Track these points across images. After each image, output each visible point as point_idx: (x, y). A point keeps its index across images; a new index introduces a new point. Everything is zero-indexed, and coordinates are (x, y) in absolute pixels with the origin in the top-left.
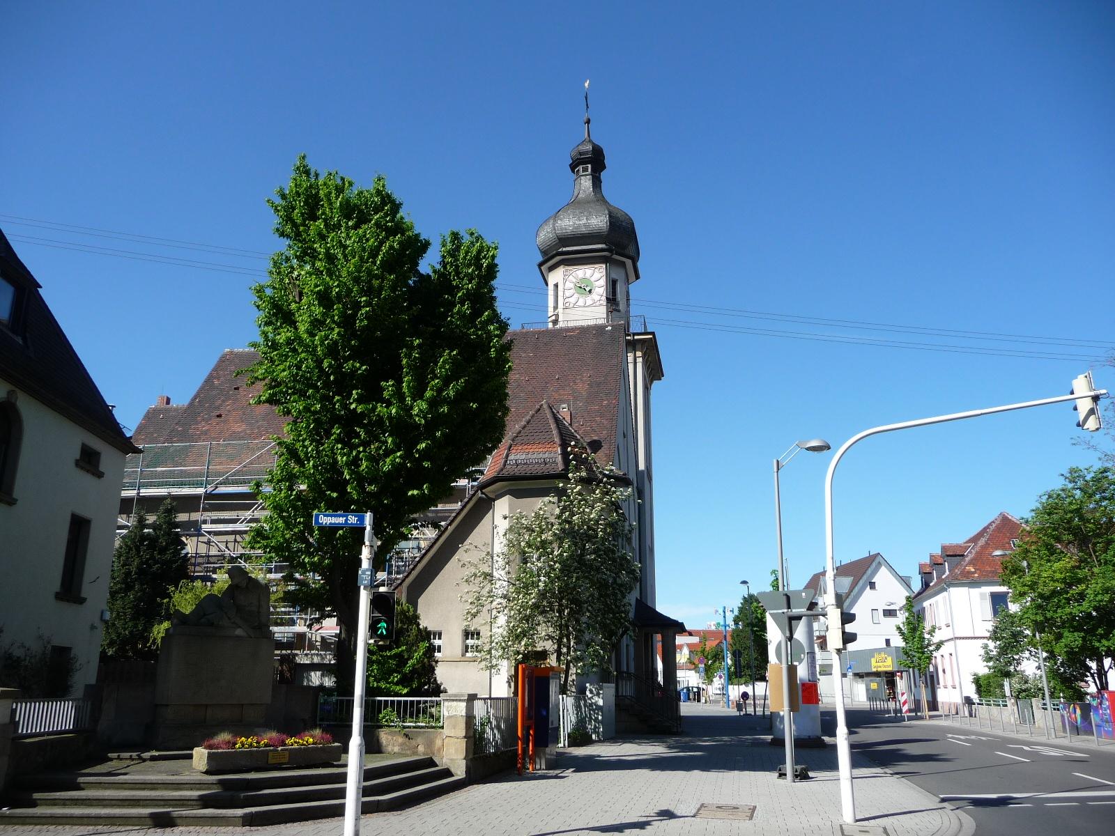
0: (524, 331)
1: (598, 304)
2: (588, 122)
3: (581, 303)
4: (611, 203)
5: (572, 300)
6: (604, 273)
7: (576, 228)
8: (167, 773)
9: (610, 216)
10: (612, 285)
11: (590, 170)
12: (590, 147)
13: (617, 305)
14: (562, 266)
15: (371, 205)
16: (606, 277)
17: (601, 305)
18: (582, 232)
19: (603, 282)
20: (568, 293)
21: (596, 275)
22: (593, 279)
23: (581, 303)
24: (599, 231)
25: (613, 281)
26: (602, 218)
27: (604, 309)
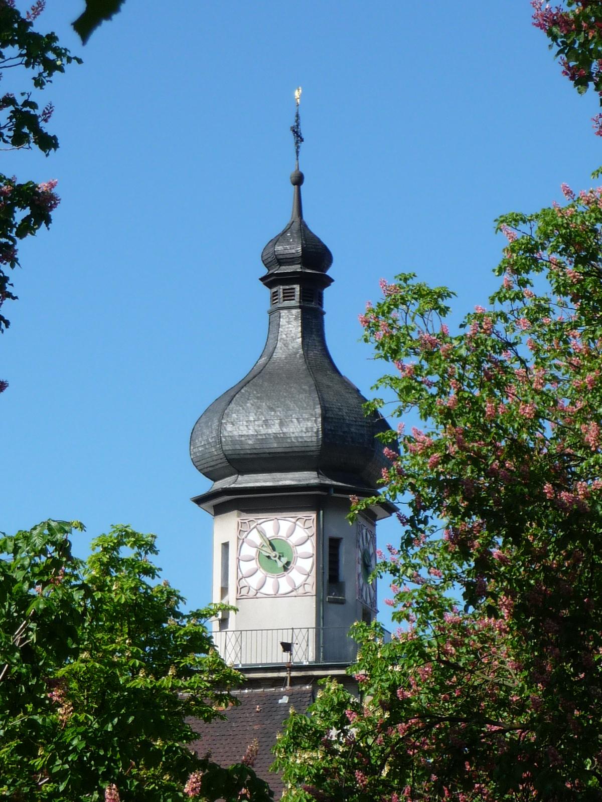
1: (301, 591)
2: (299, 180)
6: (314, 530)
19: (310, 548)
23: (268, 589)
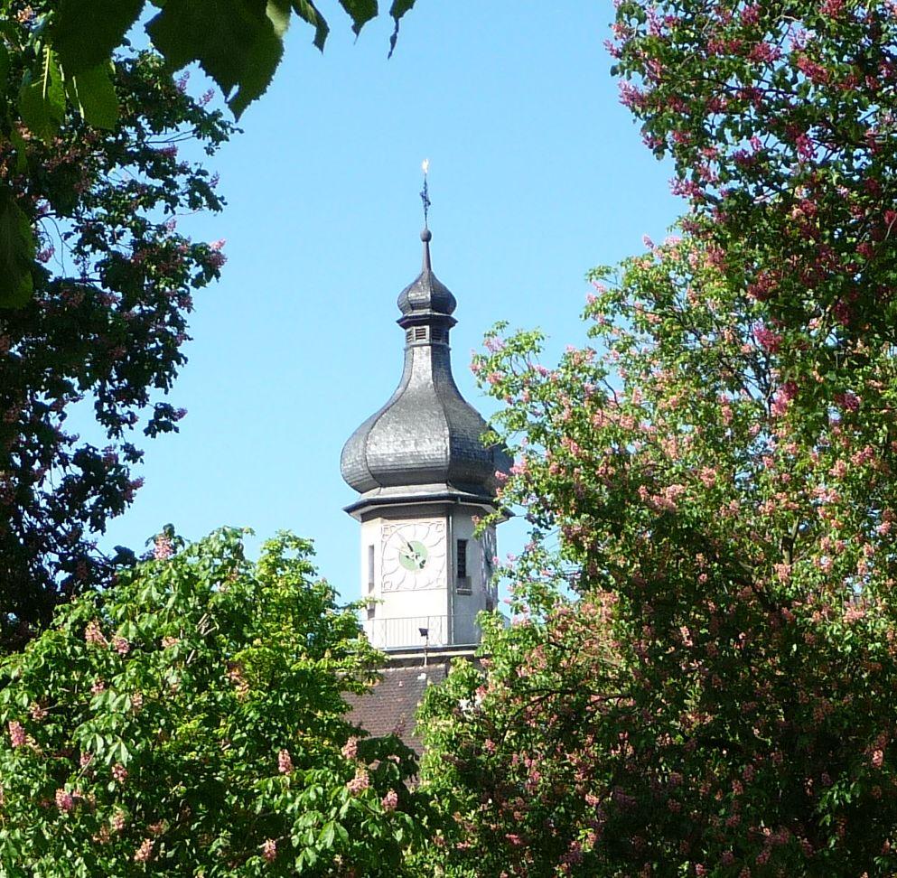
0: (139, 460)
1: (434, 585)
3: (409, 584)
4: (467, 401)
5: (395, 579)
7: (400, 459)
8: (410, 491)
9: (452, 439)
10: (459, 550)
11: (428, 336)
12: (426, 296)
13: (468, 584)
14: (379, 519)
15: (310, 630)
16: (448, 541)
17: (438, 588)
18: (408, 467)
19: (443, 548)
20: (389, 567)
21: (432, 534)
22: (426, 543)
23: (409, 584)
24: (434, 465)
25: (459, 541)
26: (439, 444)
27: (442, 597)
